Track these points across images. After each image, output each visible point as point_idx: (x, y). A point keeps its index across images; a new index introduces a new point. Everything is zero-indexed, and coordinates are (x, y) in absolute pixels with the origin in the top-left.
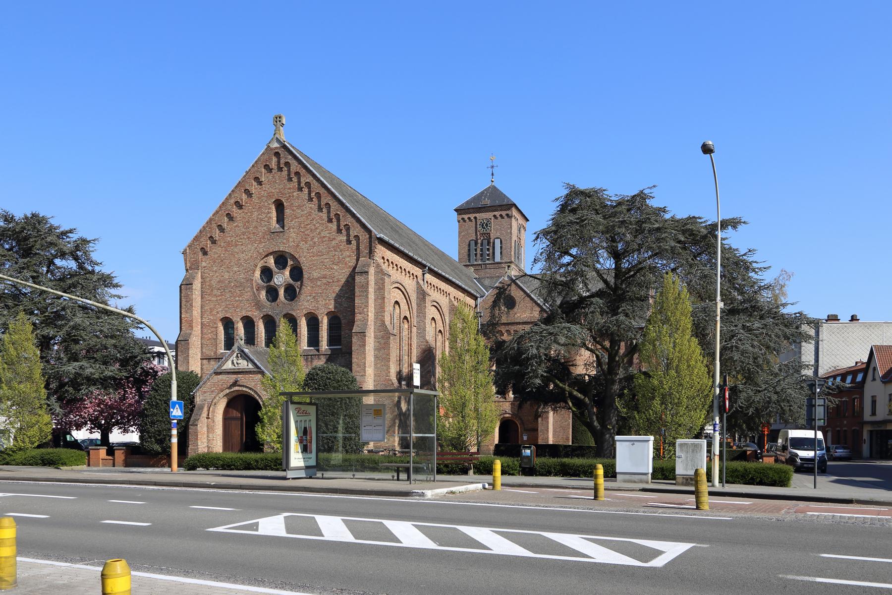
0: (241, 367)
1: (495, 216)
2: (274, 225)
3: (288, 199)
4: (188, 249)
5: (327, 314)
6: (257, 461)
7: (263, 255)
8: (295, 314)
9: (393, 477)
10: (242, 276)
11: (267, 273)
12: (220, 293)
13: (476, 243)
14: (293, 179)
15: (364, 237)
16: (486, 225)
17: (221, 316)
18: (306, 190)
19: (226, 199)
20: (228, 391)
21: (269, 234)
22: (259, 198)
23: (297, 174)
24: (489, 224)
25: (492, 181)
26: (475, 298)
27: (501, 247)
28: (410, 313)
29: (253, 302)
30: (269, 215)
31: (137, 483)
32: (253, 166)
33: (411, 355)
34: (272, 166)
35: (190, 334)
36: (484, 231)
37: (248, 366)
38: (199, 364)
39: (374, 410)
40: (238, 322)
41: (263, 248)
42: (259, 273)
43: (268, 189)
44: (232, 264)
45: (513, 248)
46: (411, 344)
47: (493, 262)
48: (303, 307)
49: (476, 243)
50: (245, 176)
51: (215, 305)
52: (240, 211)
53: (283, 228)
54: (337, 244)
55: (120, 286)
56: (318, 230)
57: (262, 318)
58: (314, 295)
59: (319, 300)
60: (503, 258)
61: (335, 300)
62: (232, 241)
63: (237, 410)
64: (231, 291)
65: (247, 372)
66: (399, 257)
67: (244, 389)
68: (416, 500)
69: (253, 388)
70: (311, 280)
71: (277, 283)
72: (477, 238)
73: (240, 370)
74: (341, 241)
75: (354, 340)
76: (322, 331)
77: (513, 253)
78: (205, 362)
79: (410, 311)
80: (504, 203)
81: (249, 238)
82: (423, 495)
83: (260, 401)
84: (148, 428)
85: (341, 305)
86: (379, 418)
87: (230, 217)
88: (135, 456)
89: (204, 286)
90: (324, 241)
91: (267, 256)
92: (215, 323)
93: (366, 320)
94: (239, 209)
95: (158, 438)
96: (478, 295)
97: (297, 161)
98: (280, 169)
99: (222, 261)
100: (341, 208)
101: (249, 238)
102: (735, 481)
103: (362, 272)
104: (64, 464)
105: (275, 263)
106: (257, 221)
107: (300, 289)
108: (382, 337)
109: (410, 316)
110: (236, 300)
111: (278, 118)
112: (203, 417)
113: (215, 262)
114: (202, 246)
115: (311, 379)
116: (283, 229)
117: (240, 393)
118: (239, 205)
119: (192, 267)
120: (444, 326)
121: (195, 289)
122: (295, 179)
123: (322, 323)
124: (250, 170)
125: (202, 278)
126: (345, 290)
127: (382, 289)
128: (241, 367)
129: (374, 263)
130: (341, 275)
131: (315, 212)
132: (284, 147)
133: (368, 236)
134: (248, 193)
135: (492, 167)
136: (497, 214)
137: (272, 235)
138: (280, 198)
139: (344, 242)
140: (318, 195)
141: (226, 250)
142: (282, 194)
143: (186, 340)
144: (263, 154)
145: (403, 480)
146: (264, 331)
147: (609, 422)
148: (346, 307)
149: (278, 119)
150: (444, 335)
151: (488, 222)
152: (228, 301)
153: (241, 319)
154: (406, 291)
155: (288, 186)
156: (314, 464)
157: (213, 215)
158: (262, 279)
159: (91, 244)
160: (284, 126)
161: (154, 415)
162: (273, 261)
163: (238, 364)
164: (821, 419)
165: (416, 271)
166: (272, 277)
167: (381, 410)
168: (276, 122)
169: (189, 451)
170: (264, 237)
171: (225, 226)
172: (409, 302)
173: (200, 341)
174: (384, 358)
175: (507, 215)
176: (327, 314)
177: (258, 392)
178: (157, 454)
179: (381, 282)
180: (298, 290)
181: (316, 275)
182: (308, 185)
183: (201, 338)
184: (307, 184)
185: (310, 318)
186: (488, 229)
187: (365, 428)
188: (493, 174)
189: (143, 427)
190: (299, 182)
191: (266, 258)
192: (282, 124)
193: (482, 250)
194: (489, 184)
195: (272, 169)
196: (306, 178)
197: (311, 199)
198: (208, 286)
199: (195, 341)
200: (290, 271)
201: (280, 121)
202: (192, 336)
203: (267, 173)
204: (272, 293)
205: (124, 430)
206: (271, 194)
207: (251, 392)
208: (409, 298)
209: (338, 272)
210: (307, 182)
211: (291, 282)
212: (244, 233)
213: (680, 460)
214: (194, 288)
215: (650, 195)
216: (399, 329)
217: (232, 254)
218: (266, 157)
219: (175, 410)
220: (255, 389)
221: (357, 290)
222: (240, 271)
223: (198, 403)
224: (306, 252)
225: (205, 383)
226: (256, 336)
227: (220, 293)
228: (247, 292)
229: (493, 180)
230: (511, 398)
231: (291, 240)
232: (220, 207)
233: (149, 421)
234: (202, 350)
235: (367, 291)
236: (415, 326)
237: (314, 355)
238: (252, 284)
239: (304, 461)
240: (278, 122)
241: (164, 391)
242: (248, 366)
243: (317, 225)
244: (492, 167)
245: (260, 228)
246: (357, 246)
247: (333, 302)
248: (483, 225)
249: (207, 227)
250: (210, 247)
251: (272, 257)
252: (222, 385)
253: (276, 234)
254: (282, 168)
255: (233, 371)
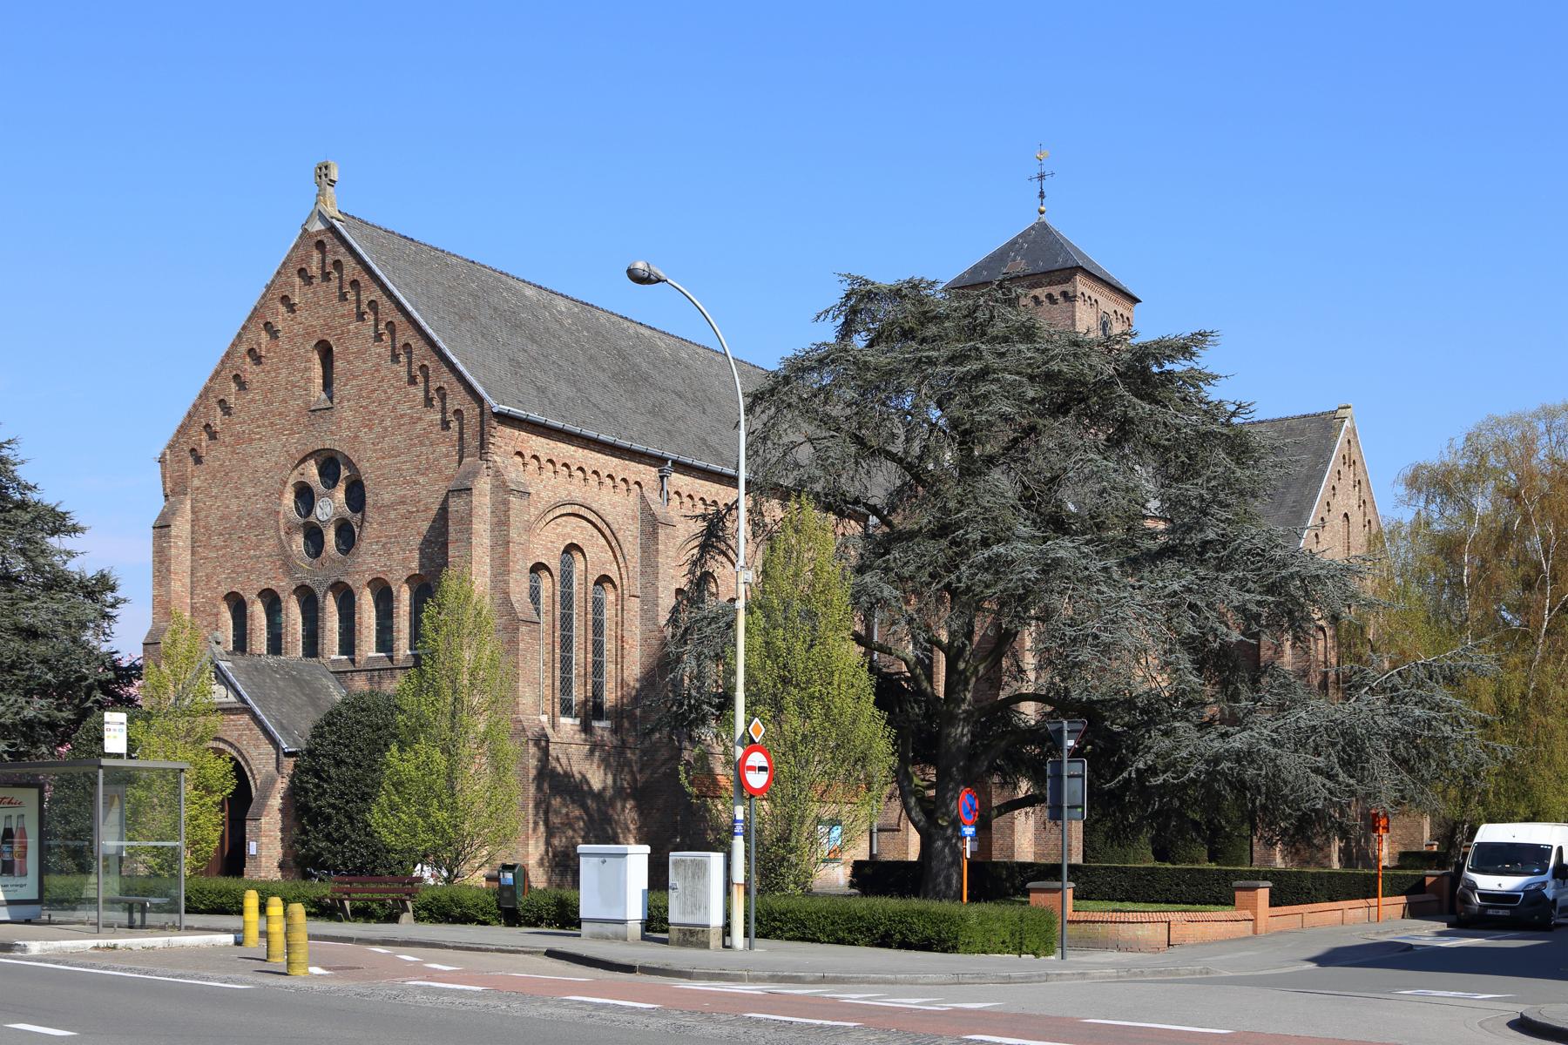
2: (317, 394)
3: (339, 339)
4: (168, 452)
5: (407, 581)
8: (350, 583)
11: (305, 496)
15: (471, 412)
17: (224, 589)
18: (370, 318)
22: (290, 339)
30: (307, 374)
32: (278, 273)
33: (622, 662)
40: (253, 603)
42: (293, 497)
43: (306, 319)
44: (244, 480)
46: (623, 637)
48: (365, 568)
50: (264, 296)
51: (215, 568)
53: (331, 399)
55: (82, 530)
58: (383, 540)
62: (244, 432)
66: (573, 448)
68: (15, 959)
71: (321, 518)
74: (431, 424)
76: (398, 617)
79: (617, 562)
80: (1056, 266)
82: (24, 949)
83: (246, 769)
89: (196, 528)
91: (303, 460)
92: (215, 605)
97: (355, 258)
98: (326, 277)
102: (857, 940)
103: (460, 490)
105: (321, 474)
106: (286, 388)
107: (361, 527)
109: (620, 574)
111: (324, 169)
115: (328, 724)
119: (175, 489)
121: (177, 537)
122: (351, 296)
123: (398, 601)
124: (273, 282)
125: (193, 512)
131: (387, 363)
132: (332, 229)
135: (1041, 177)
136: (1041, 292)
139: (437, 425)
141: (233, 452)
142: (330, 328)
143: (156, 643)
144: (296, 246)
146: (300, 620)
147: (944, 810)
149: (323, 170)
153: (259, 595)
156: (35, 896)
157: (211, 380)
160: (336, 185)
162: (316, 472)
164: (1076, 807)
168: (320, 177)
171: (231, 400)
172: (614, 543)
175: (1064, 294)
176: (407, 581)
179: (502, 507)
180: (357, 530)
181: (387, 497)
182: (373, 305)
188: (1042, 195)
192: (331, 180)
194: (1031, 220)
196: (371, 293)
198: (204, 527)
203: (305, 285)
204: (314, 536)
206: (310, 330)
209: (427, 490)
210: (372, 301)
213: (675, 894)
214: (173, 533)
216: (583, 604)
218: (301, 252)
226: (283, 631)
228: (268, 539)
229: (1043, 208)
231: (344, 425)
232: (223, 362)
237: (383, 669)
240: (323, 177)
243: (391, 391)
244: (1041, 177)
247: (416, 555)
253: (318, 413)
254: (329, 273)
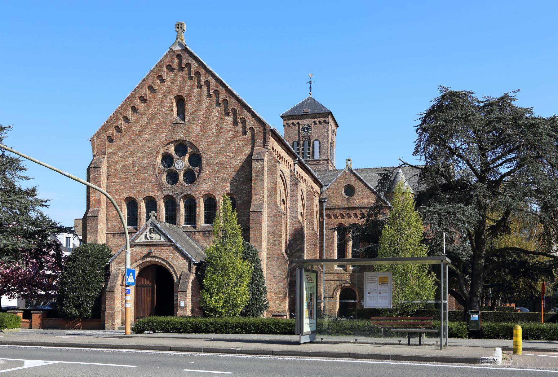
0: (154, 240)
1: (314, 122)
3: (188, 95)
4: (95, 137)
6: (207, 325)
7: (165, 143)
8: (194, 195)
9: (437, 342)
10: (146, 161)
11: (168, 159)
12: (125, 176)
13: (299, 144)
14: (193, 78)
15: (259, 129)
16: (307, 129)
17: (126, 195)
18: (205, 88)
19: (132, 94)
20: (141, 262)
21: (171, 125)
22: (162, 94)
23: (197, 73)
24: (310, 128)
25: (310, 94)
26: (320, 186)
27: (320, 148)
28: (286, 197)
29: (155, 184)
31: (150, 348)
32: (157, 66)
34: (174, 66)
35: (98, 211)
36: (305, 134)
37: (160, 239)
38: (105, 238)
39: (379, 278)
40: (141, 202)
41: (164, 137)
45: (329, 148)
47: (313, 160)
48: (202, 189)
49: (299, 144)
50: (149, 74)
51: (120, 186)
52: (144, 105)
53: (184, 120)
54: (233, 134)
56: (216, 123)
57: (163, 198)
58: (212, 178)
59: (216, 183)
60: (321, 156)
61: (231, 183)
62: (136, 130)
63: (148, 279)
64: (135, 174)
65: (159, 245)
67: (157, 260)
69: (165, 259)
70: (209, 165)
71: (177, 168)
72: (299, 139)
73: (153, 243)
74: (237, 132)
75: (252, 218)
77: (329, 152)
78: (110, 236)
81: (152, 128)
84: (67, 294)
85: (236, 187)
86: (385, 285)
87: (135, 110)
88: (51, 319)
89: (110, 169)
90: (222, 132)
91: (168, 144)
92: (120, 202)
93: (261, 201)
94: (143, 103)
95: (77, 303)
96: (323, 184)
98: (181, 69)
99: (127, 148)
100: (237, 103)
101: (152, 128)
104: (5, 327)
107: (199, 173)
108: (275, 216)
110: (139, 183)
111: (180, 25)
112: (118, 285)
113: (120, 148)
114: (109, 135)
116: (184, 121)
117: (152, 264)
118: (143, 99)
119: (98, 152)
120: (303, 209)
122: (195, 78)
124: (154, 69)
126: (241, 175)
127: (274, 174)
128: (154, 240)
129: (267, 151)
130: (238, 161)
132: (186, 50)
133: (262, 128)
134: (152, 89)
135: (310, 82)
137: (174, 126)
138: (181, 94)
139: (239, 133)
140: (217, 93)
142: (183, 90)
144: (166, 55)
145: (415, 345)
146: (164, 209)
148: (242, 190)
149: (180, 26)
150: (304, 216)
151: (309, 126)
152: (132, 183)
154: (284, 178)
155: (189, 84)
157: (119, 108)
158: (163, 164)
159: (5, 131)
161: (72, 282)
162: (174, 149)
163: (151, 237)
165: (290, 161)
166: (173, 163)
167: (387, 278)
168: (178, 28)
169: (106, 315)
170: (166, 128)
171: (130, 117)
173: (106, 217)
174: (276, 234)
177: (170, 263)
178: (75, 317)
180: (197, 174)
181: (213, 161)
182: (207, 83)
183: (107, 215)
184: (206, 82)
185: (207, 199)
186: (309, 132)
187: (368, 295)
188: (311, 88)
189: (62, 293)
190: (199, 81)
191: (168, 146)
192: (184, 30)
193: (303, 149)
195: (174, 69)
196: (205, 77)
197: (209, 95)
199: (102, 217)
200: (189, 158)
201: (181, 28)
202: (100, 213)
204: (173, 177)
205: (11, 296)
206: (173, 90)
207: (163, 262)
208: (286, 183)
210: (206, 81)
211: (191, 167)
212: (147, 124)
214: (102, 171)
215: (513, 97)
217: (136, 142)
218: (169, 58)
219: (130, 277)
220: (167, 260)
221: (253, 174)
222: (144, 157)
223: (113, 271)
224: (205, 141)
225: (120, 254)
227: (125, 176)
228: (149, 175)
229: (311, 93)
230: (350, 270)
231: (191, 130)
232: (126, 100)
233: (68, 288)
234: (107, 226)
235: (263, 176)
236: (289, 208)
238: (155, 169)
239: (310, 326)
240: (180, 28)
241: (82, 261)
242: (160, 239)
244: (310, 82)
245: (162, 120)
246: (251, 137)
248: (304, 129)
249: (113, 118)
250: (116, 136)
251: (173, 145)
252: (136, 256)
253: (177, 125)
254: (184, 68)
255: (146, 243)
